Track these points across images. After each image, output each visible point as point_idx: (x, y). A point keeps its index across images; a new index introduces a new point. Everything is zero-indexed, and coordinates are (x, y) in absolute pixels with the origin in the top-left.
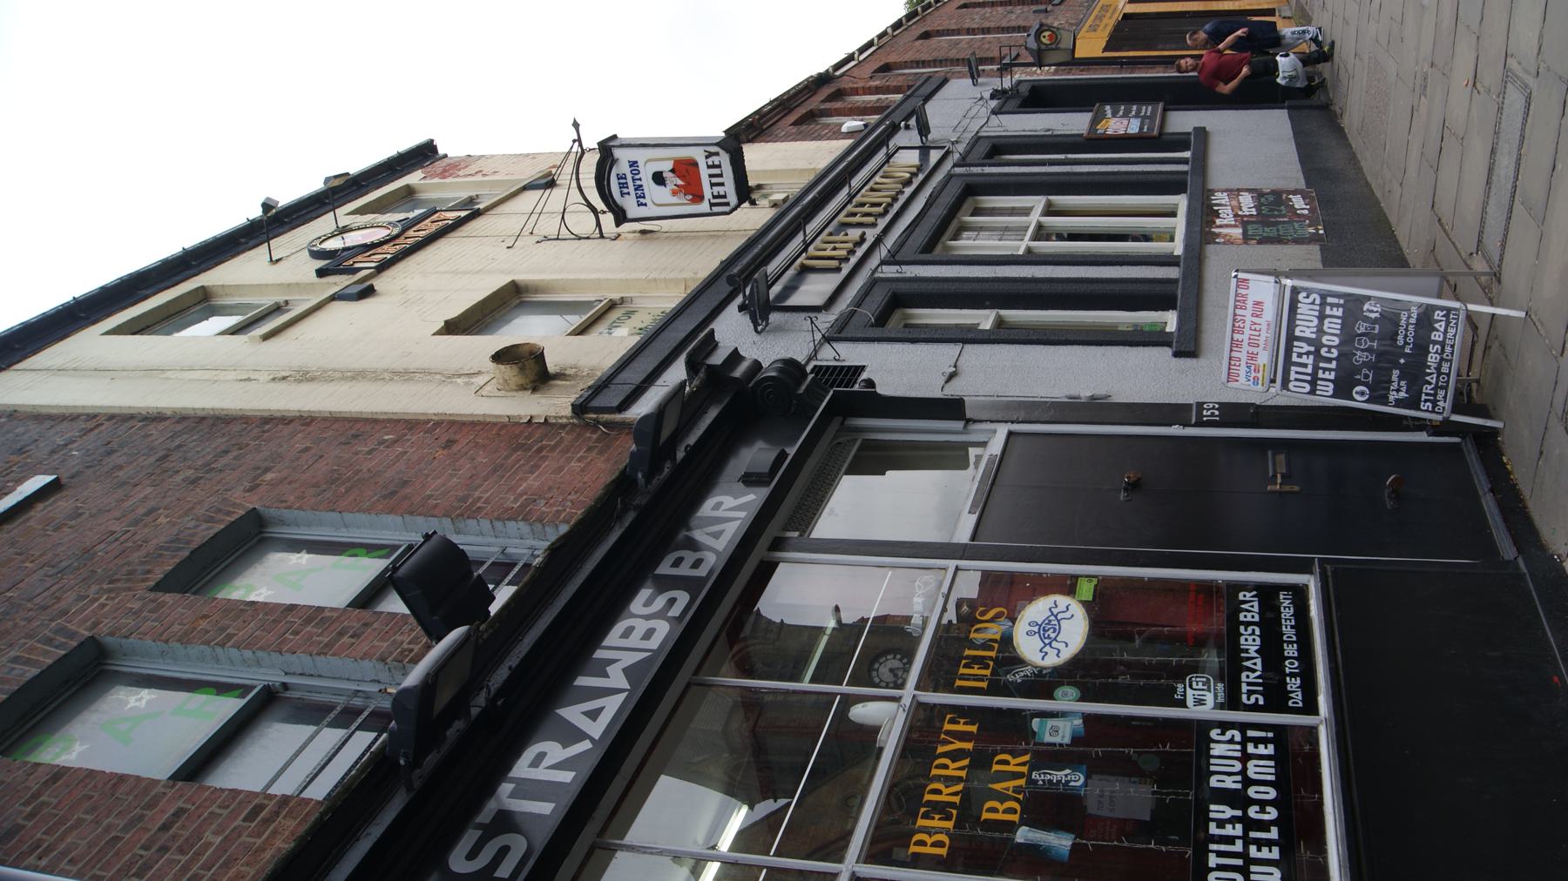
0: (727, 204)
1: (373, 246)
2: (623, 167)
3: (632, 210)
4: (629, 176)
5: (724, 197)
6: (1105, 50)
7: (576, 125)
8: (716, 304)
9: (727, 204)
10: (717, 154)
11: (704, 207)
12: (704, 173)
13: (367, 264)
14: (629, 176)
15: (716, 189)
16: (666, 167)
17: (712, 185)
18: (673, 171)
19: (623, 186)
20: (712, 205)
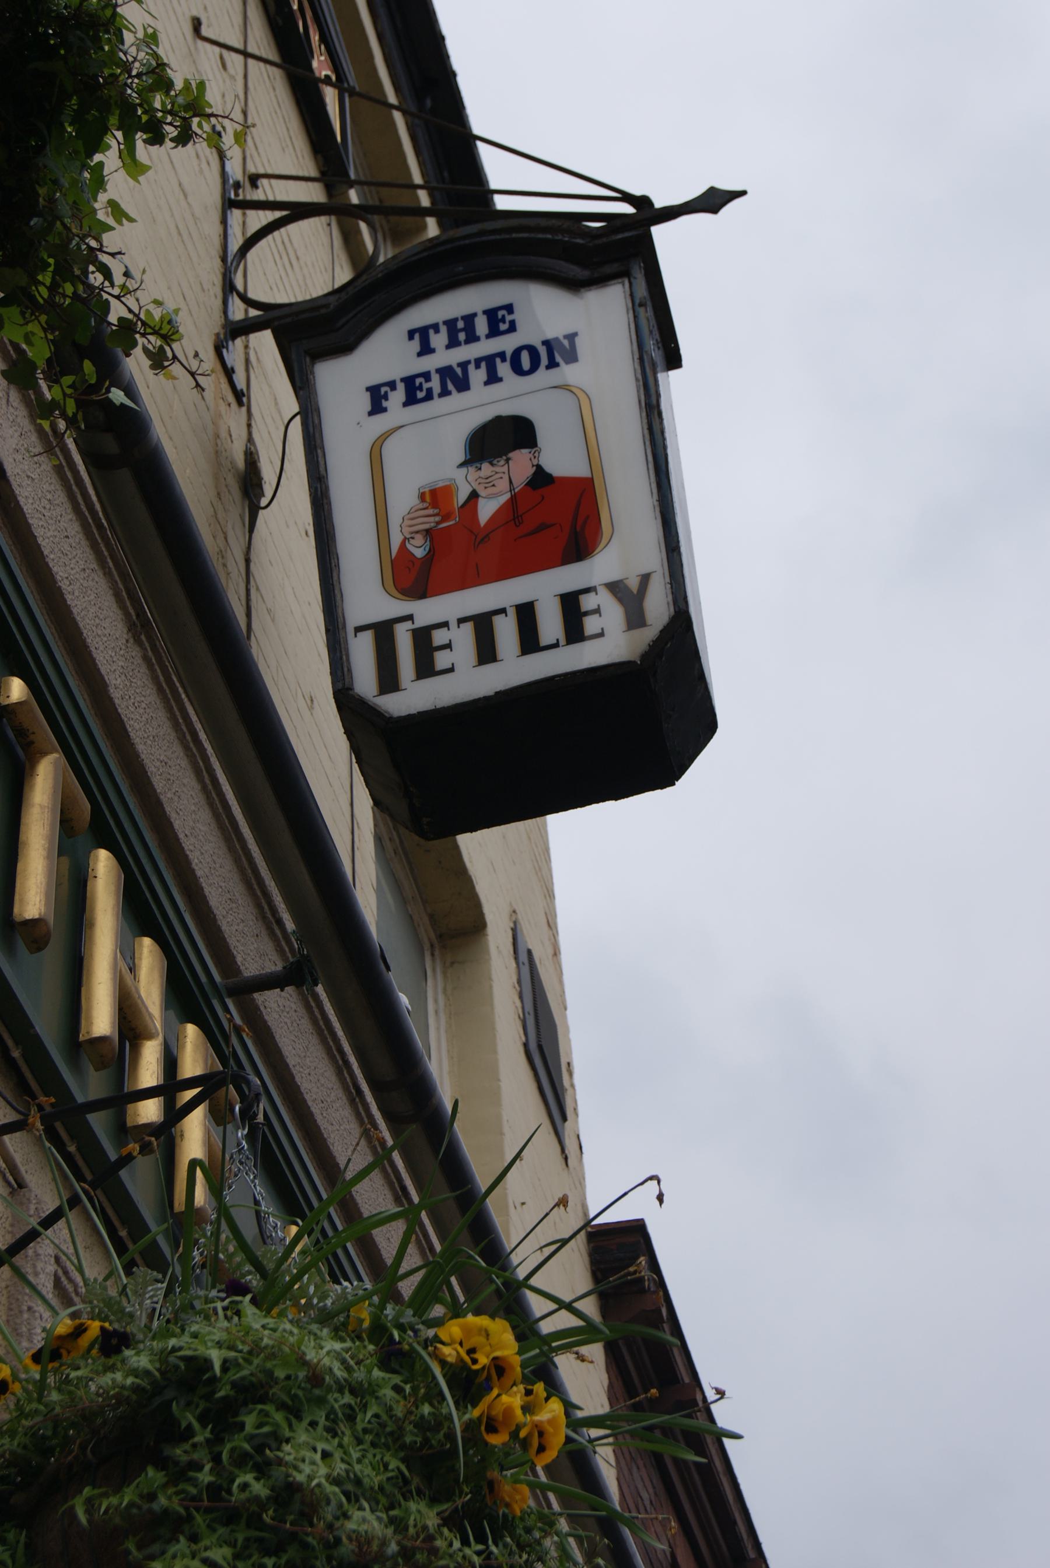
0: (389, 682)
1: (172, 215)
2: (545, 310)
3: (342, 381)
4: (507, 344)
5: (425, 669)
6: (463, 1214)
7: (713, 201)
8: (536, 1264)
9: (389, 682)
10: (635, 619)
11: (368, 599)
12: (544, 588)
13: (149, 330)
14: (507, 344)
15: (464, 639)
16: (560, 456)
17: (483, 626)
18: (541, 478)
19: (460, 330)
20: (383, 632)
